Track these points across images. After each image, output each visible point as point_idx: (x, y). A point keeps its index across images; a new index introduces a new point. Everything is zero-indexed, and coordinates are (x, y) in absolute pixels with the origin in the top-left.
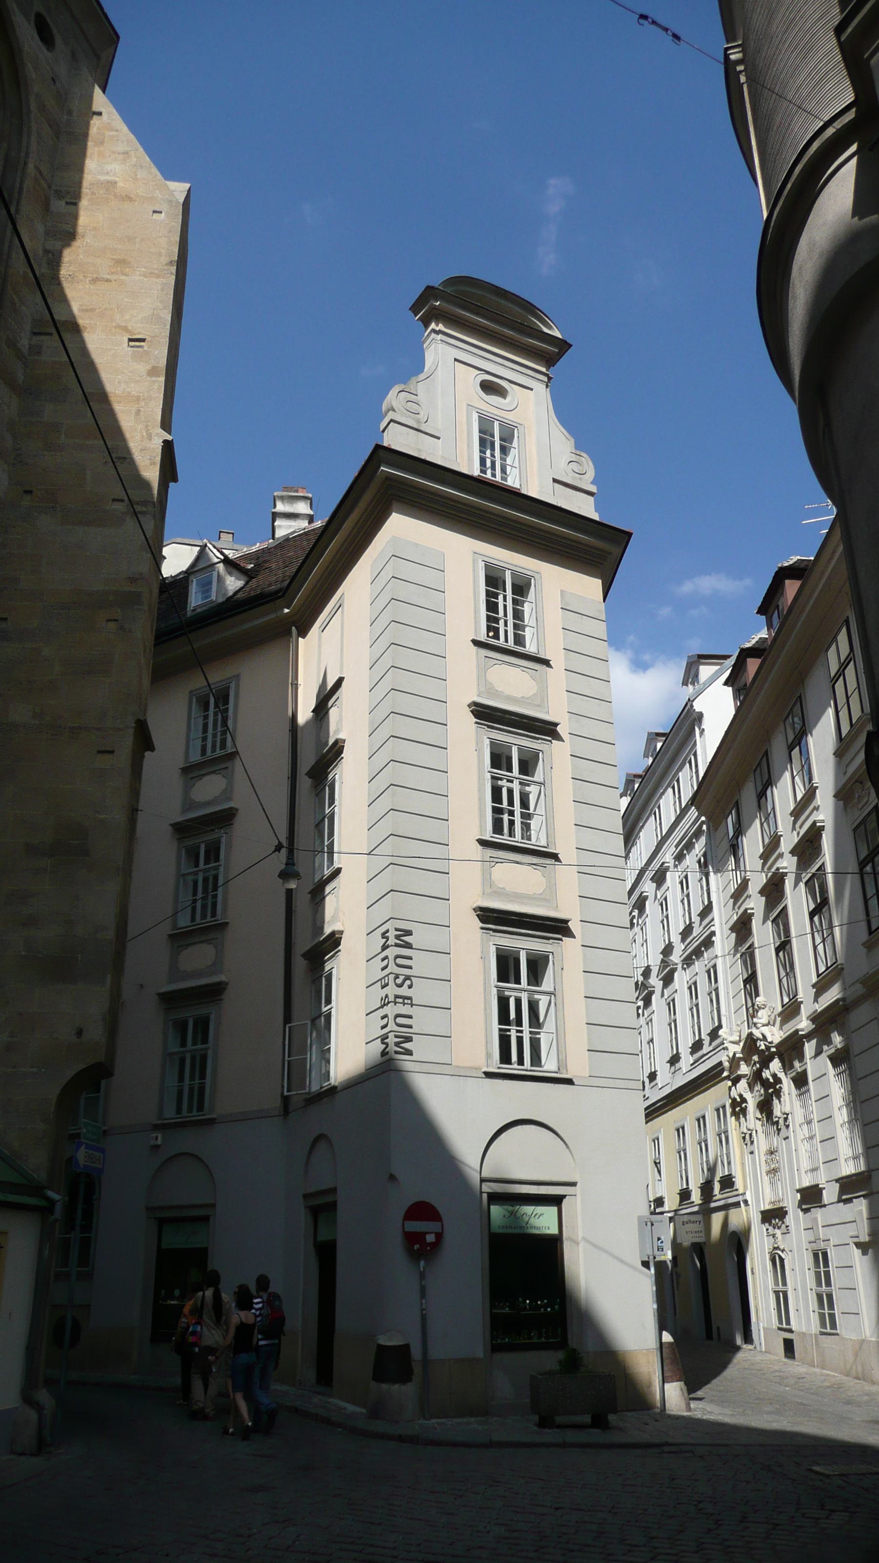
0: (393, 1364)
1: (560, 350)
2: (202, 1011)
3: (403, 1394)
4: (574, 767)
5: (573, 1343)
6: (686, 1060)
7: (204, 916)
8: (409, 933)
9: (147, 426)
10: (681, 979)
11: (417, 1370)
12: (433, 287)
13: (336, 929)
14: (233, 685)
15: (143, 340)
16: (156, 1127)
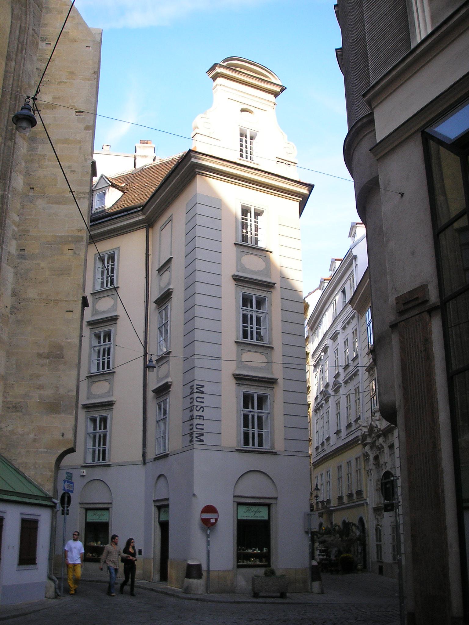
0: (194, 571)
3: (198, 584)
4: (282, 305)
5: (273, 566)
6: (343, 434)
7: (103, 368)
8: (203, 386)
9: (84, 155)
10: (342, 391)
11: (205, 574)
13: (169, 381)
14: (116, 253)
15: (82, 112)
16: (83, 467)
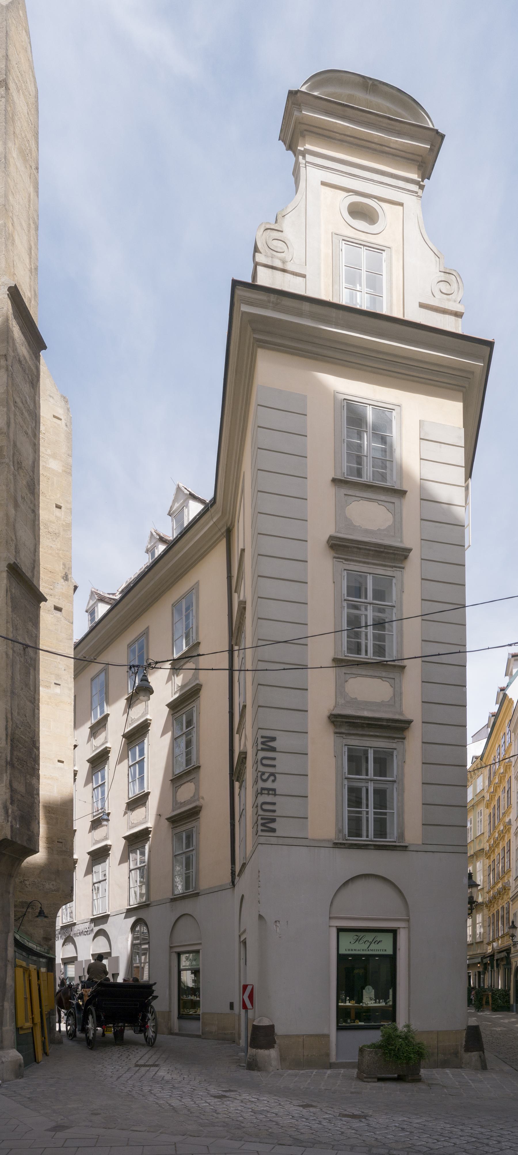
1: (432, 145)
2: (189, 826)
8: (273, 739)
12: (297, 92)
